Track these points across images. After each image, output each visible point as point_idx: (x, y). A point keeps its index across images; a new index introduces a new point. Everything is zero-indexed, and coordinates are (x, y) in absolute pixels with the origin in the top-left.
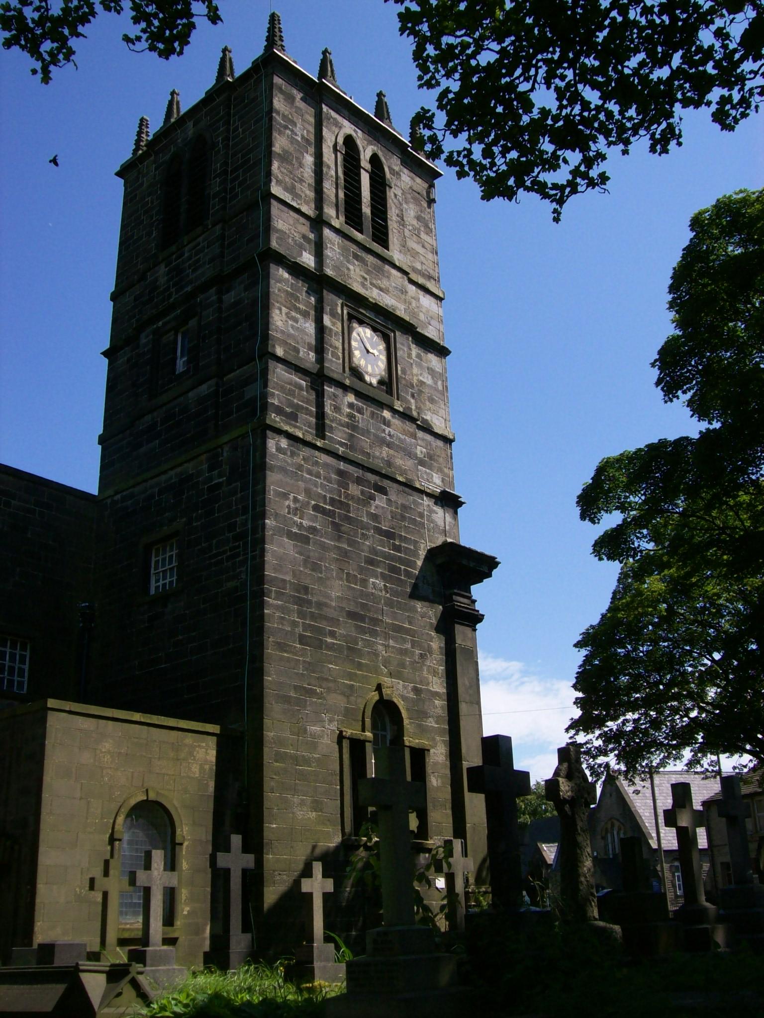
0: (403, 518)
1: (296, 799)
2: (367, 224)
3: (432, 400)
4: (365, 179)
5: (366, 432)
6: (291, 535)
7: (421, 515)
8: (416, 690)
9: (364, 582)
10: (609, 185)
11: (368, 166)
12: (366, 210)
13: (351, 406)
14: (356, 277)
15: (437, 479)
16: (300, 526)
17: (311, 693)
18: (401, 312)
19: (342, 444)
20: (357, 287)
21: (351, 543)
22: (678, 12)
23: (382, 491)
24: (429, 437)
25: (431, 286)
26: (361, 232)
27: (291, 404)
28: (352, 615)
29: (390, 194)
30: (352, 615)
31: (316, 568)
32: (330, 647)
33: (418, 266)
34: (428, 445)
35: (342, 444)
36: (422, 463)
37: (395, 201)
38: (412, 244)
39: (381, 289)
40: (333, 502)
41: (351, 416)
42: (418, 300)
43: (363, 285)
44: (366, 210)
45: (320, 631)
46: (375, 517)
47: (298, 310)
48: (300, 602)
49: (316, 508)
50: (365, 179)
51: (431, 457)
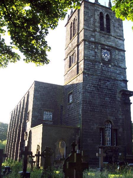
0: (114, 86)
1: (88, 139)
2: (106, 29)
3: (121, 61)
4: (105, 20)
5: (105, 71)
6: (88, 92)
7: (118, 85)
8: (116, 118)
9: (104, 99)
10: (48, 64)
11: (105, 17)
12: (105, 26)
13: (101, 66)
14: (103, 41)
15: (122, 77)
16: (90, 90)
17: (92, 120)
18: (114, 45)
19: (99, 74)
20: (103, 43)
21: (102, 92)
22: (40, 52)
23: (109, 81)
24: (120, 69)
25: (121, 38)
26: (104, 31)
27: (88, 68)
28: (101, 105)
29: (111, 21)
30: (101, 105)
31: (93, 97)
32: (96, 112)
33: (119, 35)
34: (120, 70)
35: (99, 74)
36: (118, 74)
37: (112, 23)
38: (117, 30)
39: (109, 42)
40: (97, 85)
41: (101, 68)
42: (118, 41)
43: (104, 42)
44: (105, 26)
45: (95, 109)
46: (107, 86)
47: (90, 50)
48: (90, 104)
49: (94, 86)
50: (105, 20)
51: (121, 73)
